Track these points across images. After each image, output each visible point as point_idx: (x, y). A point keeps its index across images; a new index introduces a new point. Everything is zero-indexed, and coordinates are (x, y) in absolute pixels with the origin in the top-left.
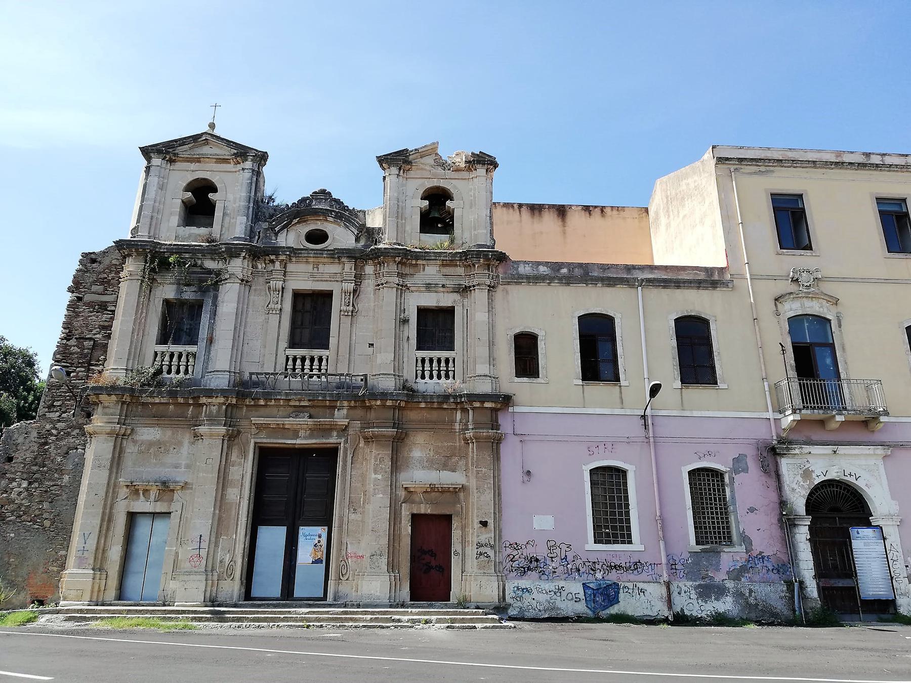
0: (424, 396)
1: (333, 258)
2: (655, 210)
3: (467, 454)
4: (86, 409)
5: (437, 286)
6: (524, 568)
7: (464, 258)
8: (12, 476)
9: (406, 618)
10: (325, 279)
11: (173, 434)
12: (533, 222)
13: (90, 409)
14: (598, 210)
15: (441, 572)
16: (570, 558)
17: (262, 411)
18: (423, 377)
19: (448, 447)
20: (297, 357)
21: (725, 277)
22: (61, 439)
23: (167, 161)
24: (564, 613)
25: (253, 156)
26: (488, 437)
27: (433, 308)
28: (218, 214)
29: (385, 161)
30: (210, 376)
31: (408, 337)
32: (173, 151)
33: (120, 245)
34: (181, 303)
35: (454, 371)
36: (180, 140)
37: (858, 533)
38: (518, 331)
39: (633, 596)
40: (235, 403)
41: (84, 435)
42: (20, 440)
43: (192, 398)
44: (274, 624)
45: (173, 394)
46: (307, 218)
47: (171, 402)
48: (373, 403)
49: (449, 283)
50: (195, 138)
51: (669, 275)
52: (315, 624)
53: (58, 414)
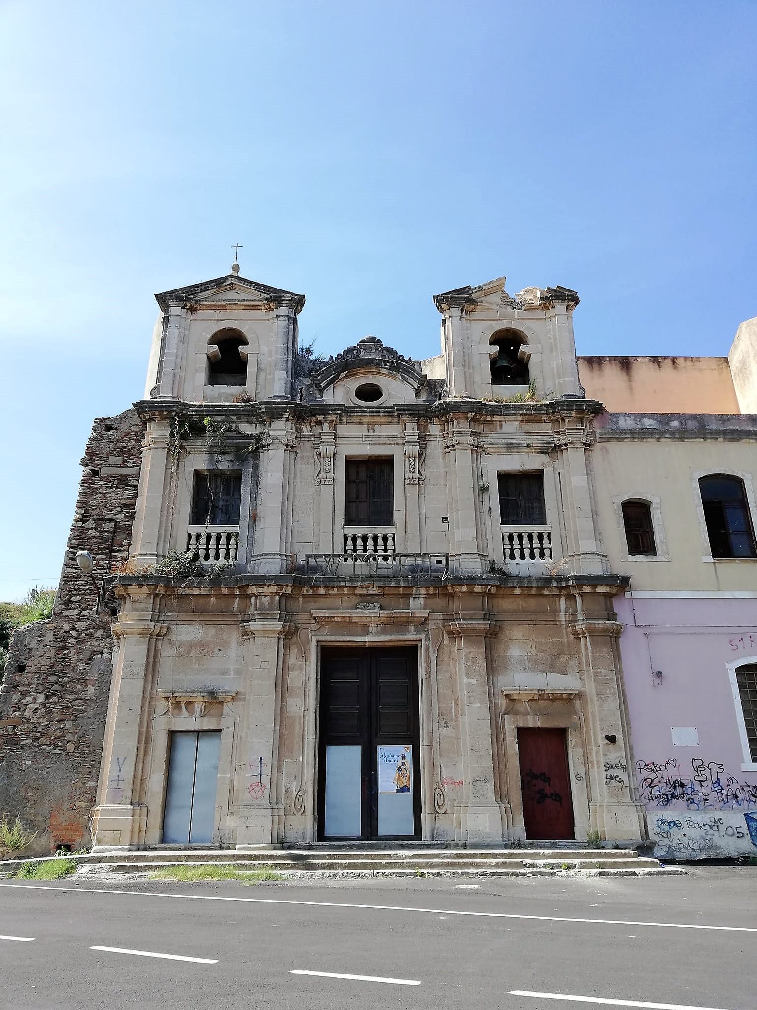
0: (520, 580)
1: (391, 416)
2: (740, 358)
3: (579, 651)
4: (110, 605)
5: (520, 445)
7: (551, 411)
8: (25, 689)
9: (540, 862)
10: (384, 442)
11: (217, 632)
13: (115, 605)
14: (668, 362)
15: (558, 801)
16: (724, 782)
17: (322, 602)
18: (512, 557)
19: (554, 643)
20: (357, 535)
22: (83, 642)
23: (187, 309)
25: (289, 300)
26: (605, 630)
27: (515, 473)
28: (251, 369)
29: (444, 301)
30: (257, 561)
31: (490, 508)
32: (194, 297)
33: (140, 407)
34: (215, 475)
35: (550, 549)
36: (202, 284)
38: (626, 498)
40: (291, 593)
41: (109, 636)
42: (33, 644)
43: (238, 588)
44: (378, 871)
45: (215, 583)
46: (357, 371)
47: (212, 593)
48: (458, 589)
49: (536, 442)
50: (219, 282)
52: (430, 871)
53: (77, 611)
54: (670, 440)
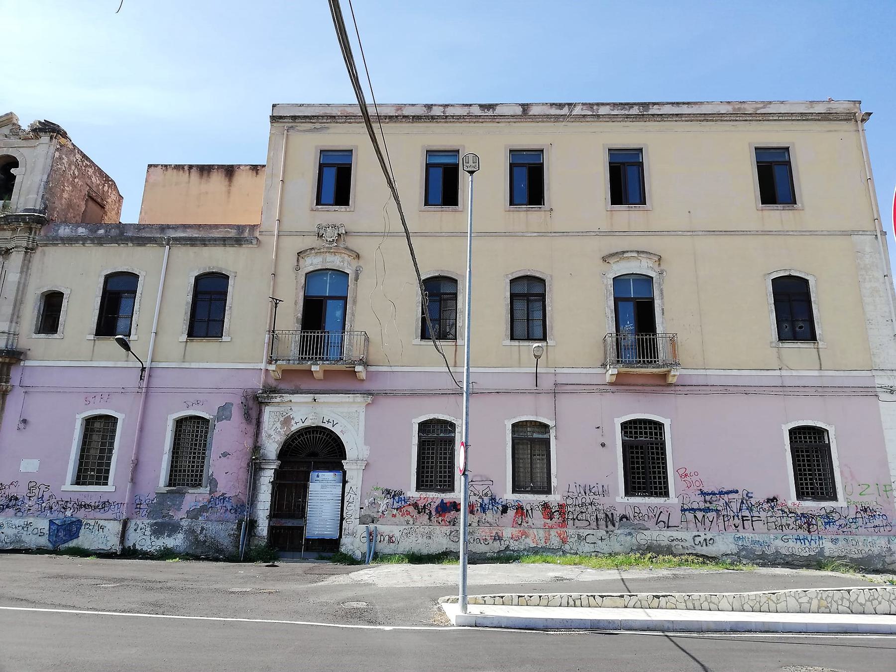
6: (3, 506)
12: (200, 183)
16: (46, 497)
21: (255, 234)
24: (27, 546)
37: (318, 476)
39: (92, 532)
51: (200, 233)
54: (92, 245)
